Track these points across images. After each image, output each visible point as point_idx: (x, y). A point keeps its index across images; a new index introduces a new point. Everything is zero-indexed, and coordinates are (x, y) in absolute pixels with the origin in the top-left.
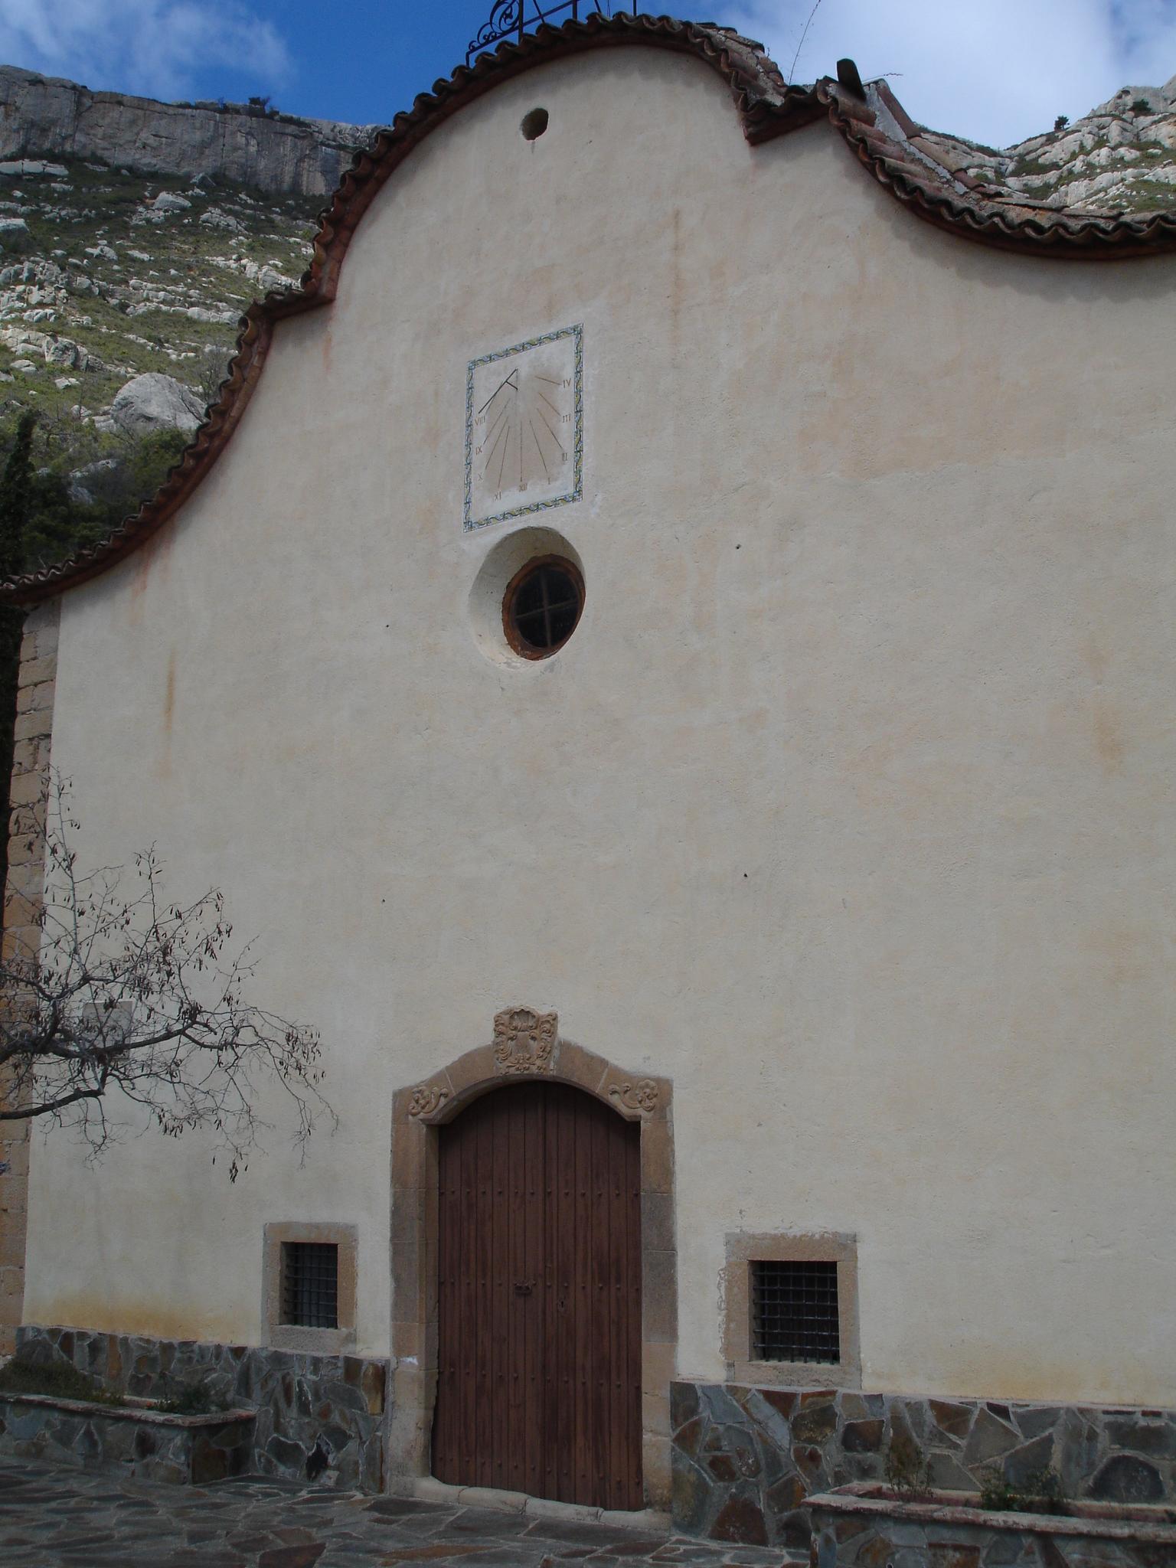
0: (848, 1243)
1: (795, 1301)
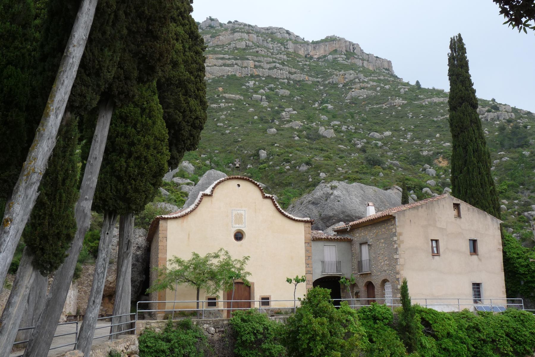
0: (270, 296)
1: (265, 301)
